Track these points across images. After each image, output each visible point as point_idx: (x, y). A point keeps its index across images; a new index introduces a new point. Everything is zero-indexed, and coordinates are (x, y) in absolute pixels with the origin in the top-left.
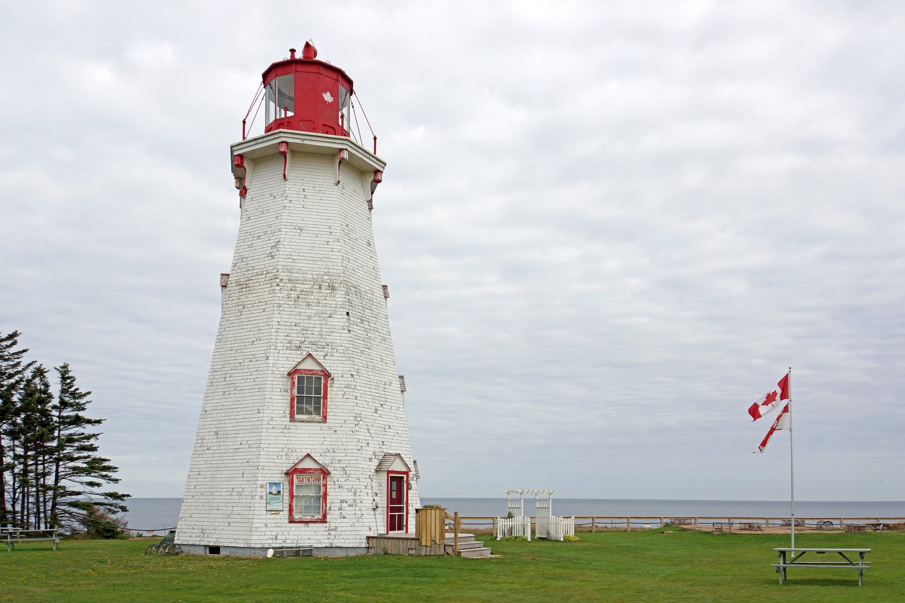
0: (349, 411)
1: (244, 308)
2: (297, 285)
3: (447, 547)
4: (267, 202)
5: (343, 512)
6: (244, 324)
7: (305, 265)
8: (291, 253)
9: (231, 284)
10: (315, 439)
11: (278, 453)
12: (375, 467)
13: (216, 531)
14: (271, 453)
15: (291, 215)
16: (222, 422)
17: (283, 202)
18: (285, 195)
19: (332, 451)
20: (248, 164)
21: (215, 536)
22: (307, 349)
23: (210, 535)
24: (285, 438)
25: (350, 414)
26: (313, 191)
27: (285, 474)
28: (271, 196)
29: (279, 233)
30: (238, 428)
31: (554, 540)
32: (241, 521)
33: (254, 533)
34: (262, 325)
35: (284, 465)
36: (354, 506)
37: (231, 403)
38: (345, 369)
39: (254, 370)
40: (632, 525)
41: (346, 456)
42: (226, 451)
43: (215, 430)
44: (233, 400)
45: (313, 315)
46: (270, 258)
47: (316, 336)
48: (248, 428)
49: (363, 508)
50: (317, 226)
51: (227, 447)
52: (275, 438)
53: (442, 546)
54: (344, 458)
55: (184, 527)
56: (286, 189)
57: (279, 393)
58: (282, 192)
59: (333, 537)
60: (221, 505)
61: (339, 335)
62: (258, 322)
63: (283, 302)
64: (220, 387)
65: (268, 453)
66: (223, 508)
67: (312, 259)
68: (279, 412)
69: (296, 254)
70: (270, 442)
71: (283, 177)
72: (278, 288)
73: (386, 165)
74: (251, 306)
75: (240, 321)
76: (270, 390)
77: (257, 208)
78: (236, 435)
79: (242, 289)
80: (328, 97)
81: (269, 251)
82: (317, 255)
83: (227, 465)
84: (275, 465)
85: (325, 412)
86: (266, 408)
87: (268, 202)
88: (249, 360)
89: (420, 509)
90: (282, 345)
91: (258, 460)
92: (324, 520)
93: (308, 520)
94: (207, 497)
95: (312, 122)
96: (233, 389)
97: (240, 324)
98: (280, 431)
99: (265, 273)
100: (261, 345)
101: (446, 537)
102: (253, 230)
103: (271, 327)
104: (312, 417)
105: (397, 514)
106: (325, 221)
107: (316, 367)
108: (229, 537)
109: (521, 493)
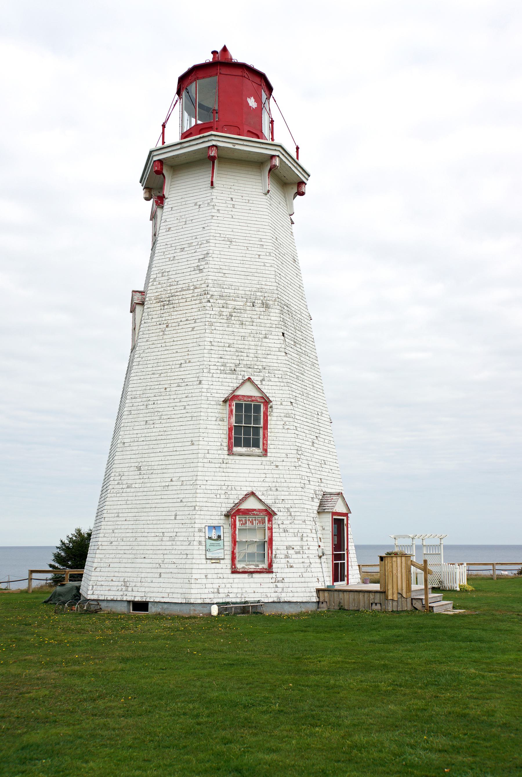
0: (290, 443)
1: (167, 326)
2: (228, 302)
3: (414, 602)
4: (190, 212)
5: (290, 561)
6: (167, 344)
7: (236, 280)
8: (221, 267)
9: (150, 300)
10: (256, 475)
11: (216, 492)
12: (317, 508)
13: (143, 583)
14: (209, 492)
15: (220, 225)
16: (146, 455)
17: (210, 211)
18: (213, 203)
19: (274, 489)
20: (167, 170)
21: (143, 589)
22: (242, 373)
23: (135, 589)
24: (223, 474)
25: (292, 447)
26: (241, 201)
27: (225, 515)
28: (196, 204)
29: (208, 245)
30: (167, 462)
31: (449, 590)
32: (176, 571)
33: (193, 586)
34: (191, 345)
35: (224, 505)
36: (301, 553)
37: (157, 434)
38: (284, 396)
39: (184, 396)
40: (497, 572)
41: (290, 495)
42: (152, 489)
43: (136, 464)
44: (158, 430)
45: (247, 335)
46: (198, 272)
47: (251, 359)
48: (179, 462)
49: (311, 556)
50: (247, 238)
51: (153, 485)
52: (213, 474)
53: (409, 600)
54: (288, 497)
55: (100, 579)
56: (213, 197)
57: (214, 423)
58: (209, 201)
59: (280, 590)
60: (148, 552)
61: (275, 357)
62: (185, 342)
63: (214, 320)
64: (141, 415)
65: (206, 491)
66: (151, 556)
67: (243, 273)
68: (215, 444)
69: (227, 268)
70: (207, 478)
71: (210, 185)
72: (209, 304)
73: (309, 176)
74: (177, 324)
75: (163, 341)
76: (205, 418)
77: (179, 218)
78: (164, 471)
79: (164, 306)
80: (252, 102)
81: (196, 265)
82: (249, 270)
83: (154, 506)
84: (213, 505)
85: (265, 444)
86: (201, 439)
87: (192, 212)
88: (176, 385)
89: (385, 557)
90: (216, 367)
91: (194, 500)
92: (269, 570)
93: (252, 570)
94: (129, 543)
96: (158, 418)
97: (163, 345)
98: (217, 465)
99: (192, 288)
100: (191, 368)
101: (412, 590)
102: (174, 242)
103: (202, 347)
104: (251, 450)
105: (339, 562)
106: (255, 233)
107: (255, 393)
108: (160, 590)
109: (413, 539)
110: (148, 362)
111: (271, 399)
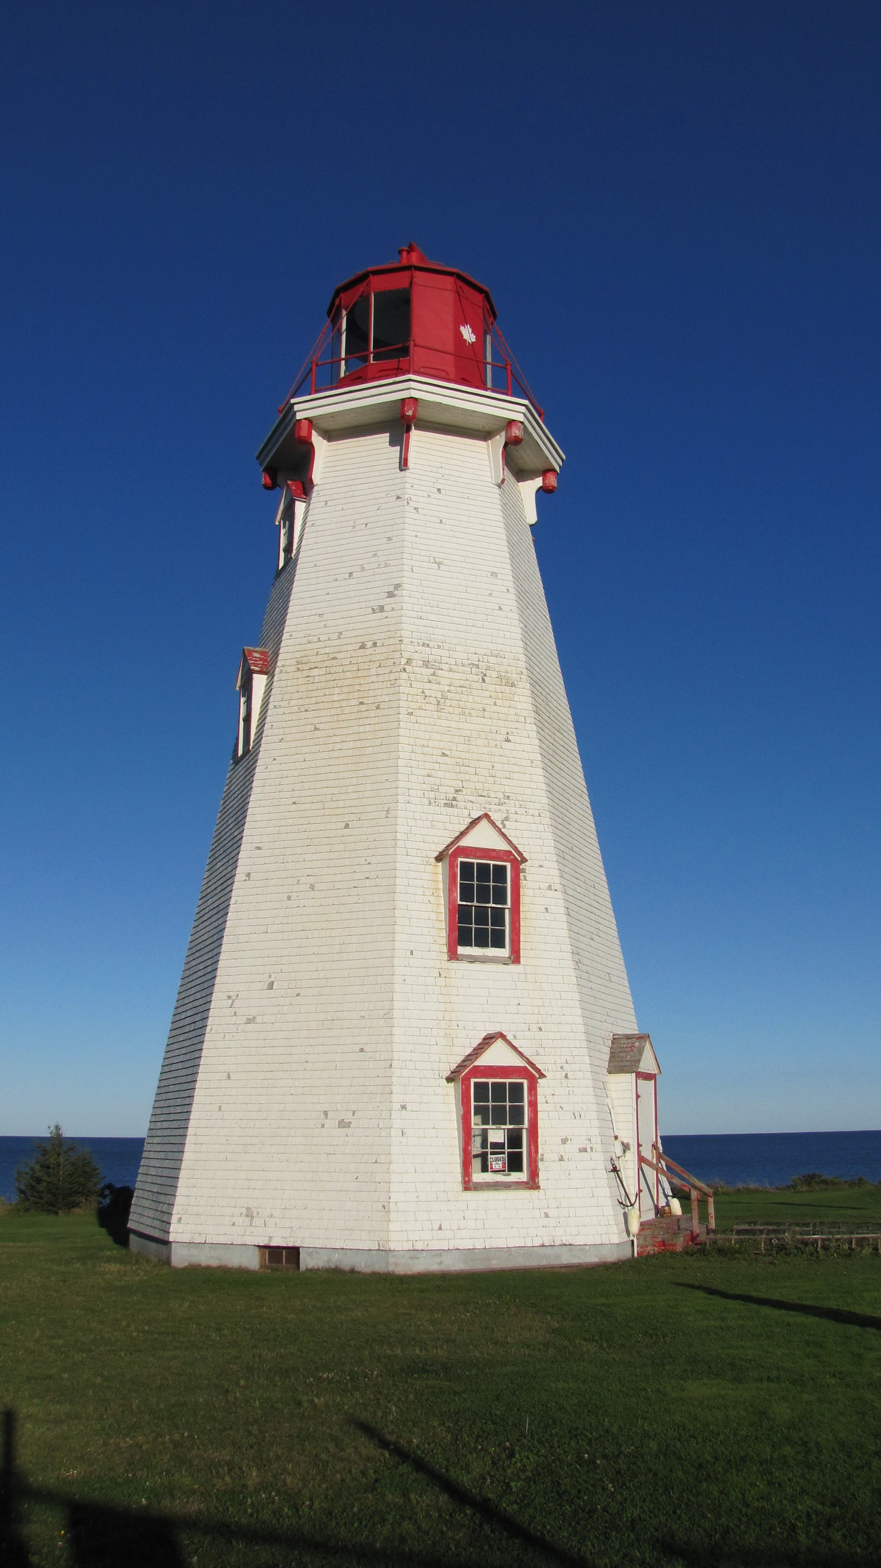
19: (534, 1027)
36: (589, 1150)
47: (483, 779)
95: (444, 373)
110: (286, 781)
111: (525, 855)
